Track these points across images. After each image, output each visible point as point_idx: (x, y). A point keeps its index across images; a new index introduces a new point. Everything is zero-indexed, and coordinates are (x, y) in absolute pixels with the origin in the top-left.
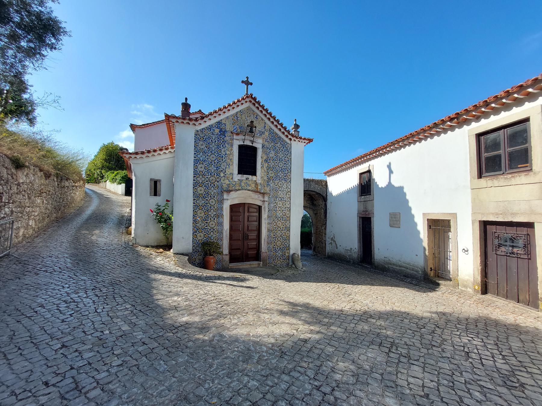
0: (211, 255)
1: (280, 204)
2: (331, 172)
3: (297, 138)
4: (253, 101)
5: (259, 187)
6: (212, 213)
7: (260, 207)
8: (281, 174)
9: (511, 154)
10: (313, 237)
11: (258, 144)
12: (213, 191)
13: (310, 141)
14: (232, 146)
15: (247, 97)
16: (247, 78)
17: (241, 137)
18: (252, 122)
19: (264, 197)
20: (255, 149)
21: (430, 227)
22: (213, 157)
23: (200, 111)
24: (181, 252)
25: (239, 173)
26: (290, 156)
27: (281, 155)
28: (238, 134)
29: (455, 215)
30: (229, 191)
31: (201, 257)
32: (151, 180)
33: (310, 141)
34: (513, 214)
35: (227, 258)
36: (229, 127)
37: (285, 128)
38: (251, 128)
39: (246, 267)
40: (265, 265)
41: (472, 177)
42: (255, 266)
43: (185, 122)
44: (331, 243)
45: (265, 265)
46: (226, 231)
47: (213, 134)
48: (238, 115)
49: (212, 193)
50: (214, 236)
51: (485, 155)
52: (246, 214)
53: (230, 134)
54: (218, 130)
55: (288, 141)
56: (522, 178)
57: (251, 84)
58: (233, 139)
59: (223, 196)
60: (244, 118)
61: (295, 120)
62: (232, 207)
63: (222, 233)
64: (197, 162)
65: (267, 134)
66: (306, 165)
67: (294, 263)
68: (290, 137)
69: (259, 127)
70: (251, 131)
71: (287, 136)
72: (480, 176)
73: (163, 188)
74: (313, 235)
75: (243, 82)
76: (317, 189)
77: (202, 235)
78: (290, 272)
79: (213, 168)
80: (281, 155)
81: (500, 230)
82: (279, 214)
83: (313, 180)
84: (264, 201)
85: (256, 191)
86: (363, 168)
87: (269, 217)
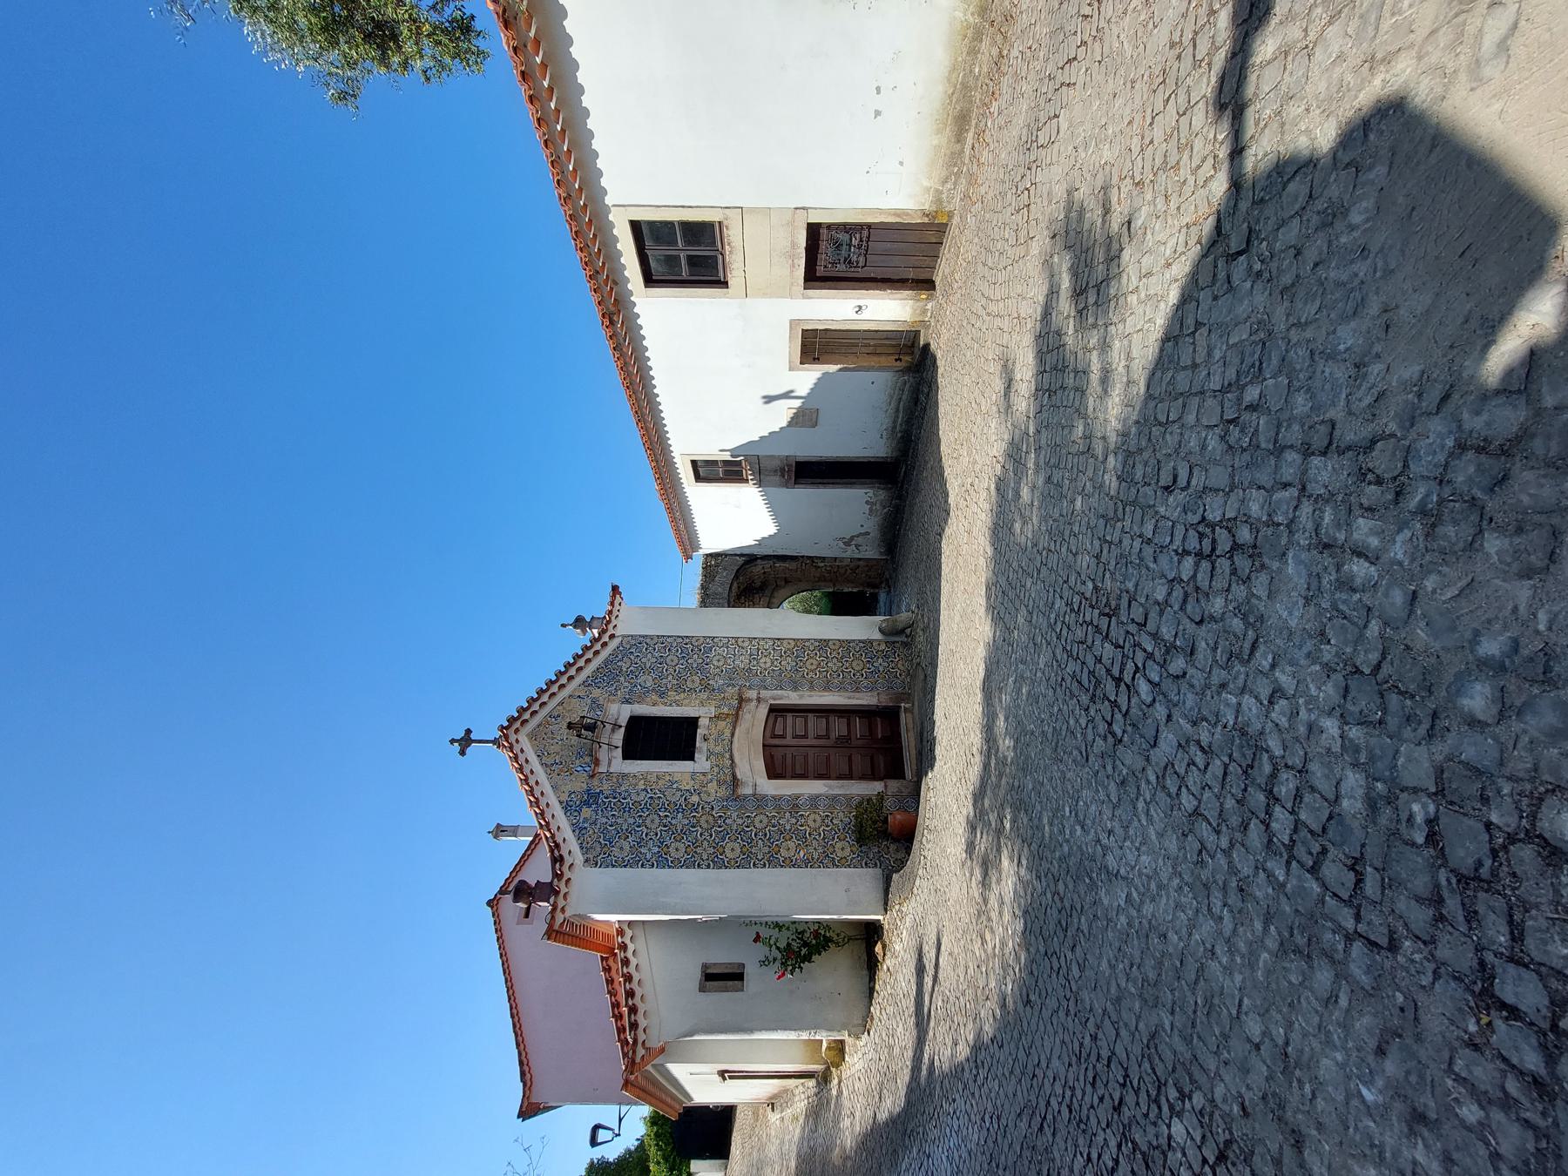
0: (886, 821)
1: (765, 662)
2: (687, 540)
3: (609, 622)
4: (518, 724)
5: (726, 710)
6: (787, 821)
7: (776, 711)
8: (695, 660)
9: (688, 242)
10: (849, 587)
11: (622, 712)
12: (734, 819)
13: (615, 589)
14: (624, 776)
15: (506, 737)
16: (453, 741)
17: (603, 754)
18: (570, 726)
19: (750, 700)
20: (635, 721)
21: (816, 360)
22: (653, 822)
23: (490, 903)
24: (880, 895)
25: (690, 757)
26: (652, 638)
27: (649, 661)
28: (597, 762)
29: (793, 323)
30: (735, 782)
31: (893, 847)
32: (702, 989)
33: (615, 589)
34: (794, 245)
35: (894, 785)
36: (579, 784)
37: (586, 649)
38: (587, 728)
39: (912, 739)
40: (907, 697)
41: (725, 296)
42: (910, 721)
43: (564, 890)
44: (857, 546)
45: (907, 697)
46: (830, 787)
47: (595, 823)
48: (550, 761)
49: (740, 821)
50: (842, 817)
51: (685, 274)
52: (789, 740)
53: (596, 782)
54: (585, 809)
55: (616, 642)
56: (733, 234)
57: (468, 732)
58: (609, 774)
59: (745, 796)
60: (556, 748)
61: (564, 626)
62: (773, 773)
63: (834, 798)
64: (662, 861)
65: (596, 693)
66: (666, 601)
67: (902, 631)
68: (606, 638)
69: (579, 710)
70: (591, 728)
71: (605, 644)
72: (725, 284)
73: (722, 955)
74: (839, 588)
75: (463, 753)
76: (724, 577)
77: (839, 845)
78: (921, 637)
79: (680, 821)
80: (649, 661)
81: (822, 259)
82: (788, 663)
83: (704, 587)
84: (759, 700)
85: (736, 718)
86: (685, 473)
87: (795, 689)
